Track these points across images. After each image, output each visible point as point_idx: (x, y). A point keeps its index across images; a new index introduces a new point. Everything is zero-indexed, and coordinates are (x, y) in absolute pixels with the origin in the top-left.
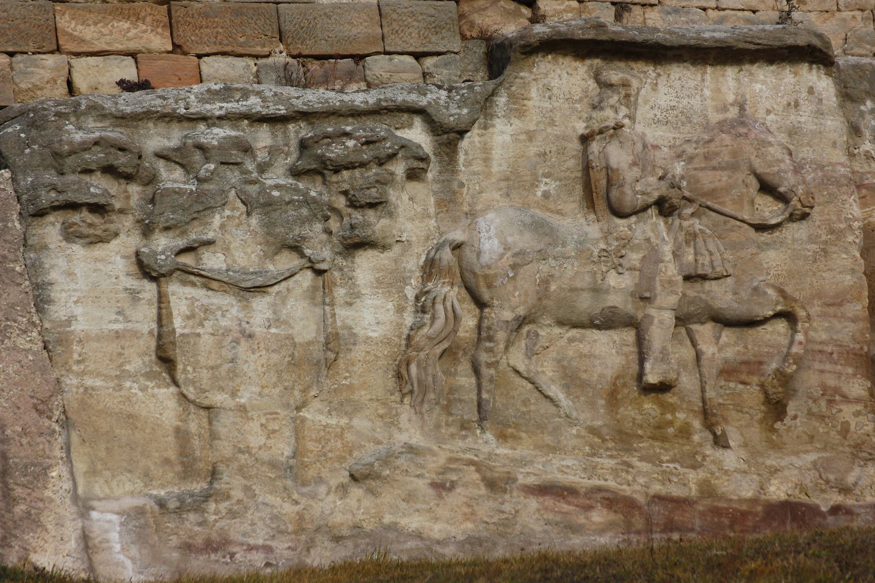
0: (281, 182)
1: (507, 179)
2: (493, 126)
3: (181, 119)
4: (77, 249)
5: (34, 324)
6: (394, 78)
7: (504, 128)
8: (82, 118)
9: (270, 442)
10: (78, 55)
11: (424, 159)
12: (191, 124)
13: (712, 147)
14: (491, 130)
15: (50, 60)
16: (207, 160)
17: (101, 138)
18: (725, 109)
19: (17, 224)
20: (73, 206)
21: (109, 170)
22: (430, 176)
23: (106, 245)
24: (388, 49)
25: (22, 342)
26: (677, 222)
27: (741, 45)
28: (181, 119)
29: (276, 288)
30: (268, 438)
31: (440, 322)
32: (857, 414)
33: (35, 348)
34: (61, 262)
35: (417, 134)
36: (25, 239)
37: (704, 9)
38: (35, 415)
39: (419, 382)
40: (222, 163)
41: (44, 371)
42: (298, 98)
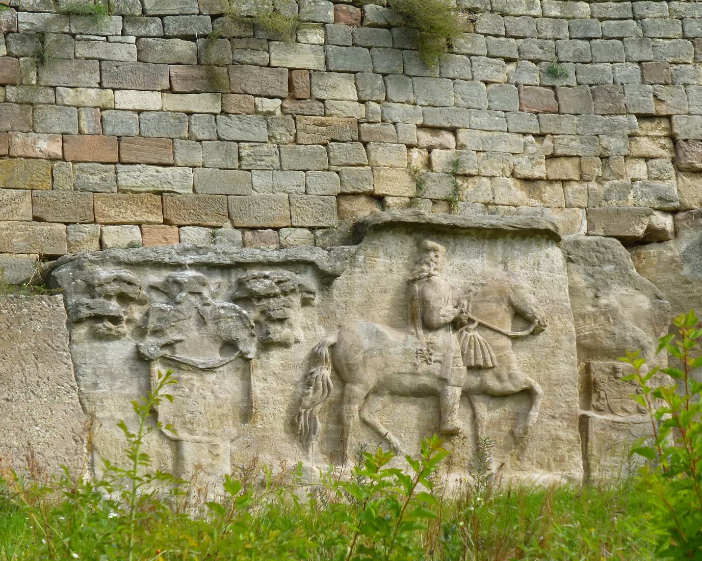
0: (226, 304)
10: (106, 224)
15: (88, 228)
16: (181, 290)
24: (294, 224)
25: (66, 399)
26: (465, 333)
27: (506, 228)
33: (74, 402)
35: (308, 280)
36: (70, 337)
42: (237, 253)
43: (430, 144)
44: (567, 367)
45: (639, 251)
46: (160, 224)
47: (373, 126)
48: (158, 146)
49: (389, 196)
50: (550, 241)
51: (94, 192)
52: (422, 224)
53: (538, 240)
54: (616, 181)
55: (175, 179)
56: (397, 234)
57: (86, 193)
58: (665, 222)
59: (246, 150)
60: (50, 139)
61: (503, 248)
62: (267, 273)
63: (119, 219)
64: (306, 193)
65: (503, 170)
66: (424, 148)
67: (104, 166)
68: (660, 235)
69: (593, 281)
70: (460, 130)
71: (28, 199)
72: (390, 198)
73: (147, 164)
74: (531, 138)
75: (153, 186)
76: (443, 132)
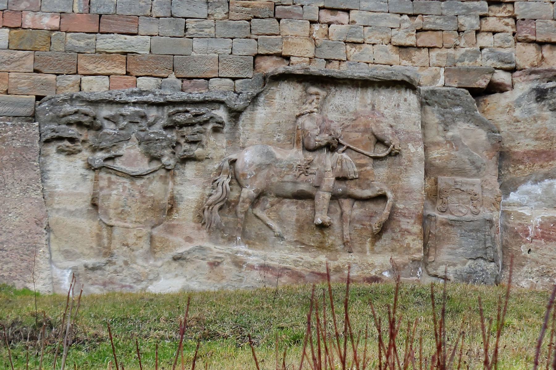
1: (261, 133)
2: (257, 110)
3: (117, 103)
4: (62, 157)
5: (39, 187)
6: (218, 88)
7: (262, 111)
8: (74, 102)
9: (137, 242)
10: (85, 75)
11: (222, 123)
12: (121, 106)
13: (356, 122)
14: (256, 111)
15: (74, 77)
17: (78, 110)
18: (366, 106)
19: (38, 145)
20: (60, 139)
21: (80, 124)
22: (225, 130)
23: (75, 156)
25: (33, 195)
27: (371, 79)
28: (117, 103)
29: (147, 176)
30: (137, 240)
31: (219, 193)
32: (414, 240)
33: (39, 197)
34: (55, 162)
35: (221, 113)
36: (40, 152)
37: (368, 63)
38: (36, 226)
39: (208, 219)
40: (130, 122)
41: (41, 207)
43: (329, 20)
44: (416, 180)
45: (485, 99)
46: (124, 75)
47: (286, 7)
48: (127, 21)
49: (293, 56)
50: (408, 90)
51: (78, 53)
52: (307, 75)
53: (398, 88)
54: (468, 49)
55: (139, 44)
56: (291, 83)
57: (73, 53)
58: (502, 77)
59: (191, 24)
60: (52, 16)
61: (373, 94)
62: (188, 109)
63: (96, 71)
64: (231, 53)
65: (383, 40)
66: (325, 23)
67: (88, 35)
68: (501, 87)
69: (443, 119)
70: (352, 11)
71: (32, 57)
72: (294, 58)
73: (119, 33)
74: (406, 17)
75: (122, 49)
76: (339, 12)
